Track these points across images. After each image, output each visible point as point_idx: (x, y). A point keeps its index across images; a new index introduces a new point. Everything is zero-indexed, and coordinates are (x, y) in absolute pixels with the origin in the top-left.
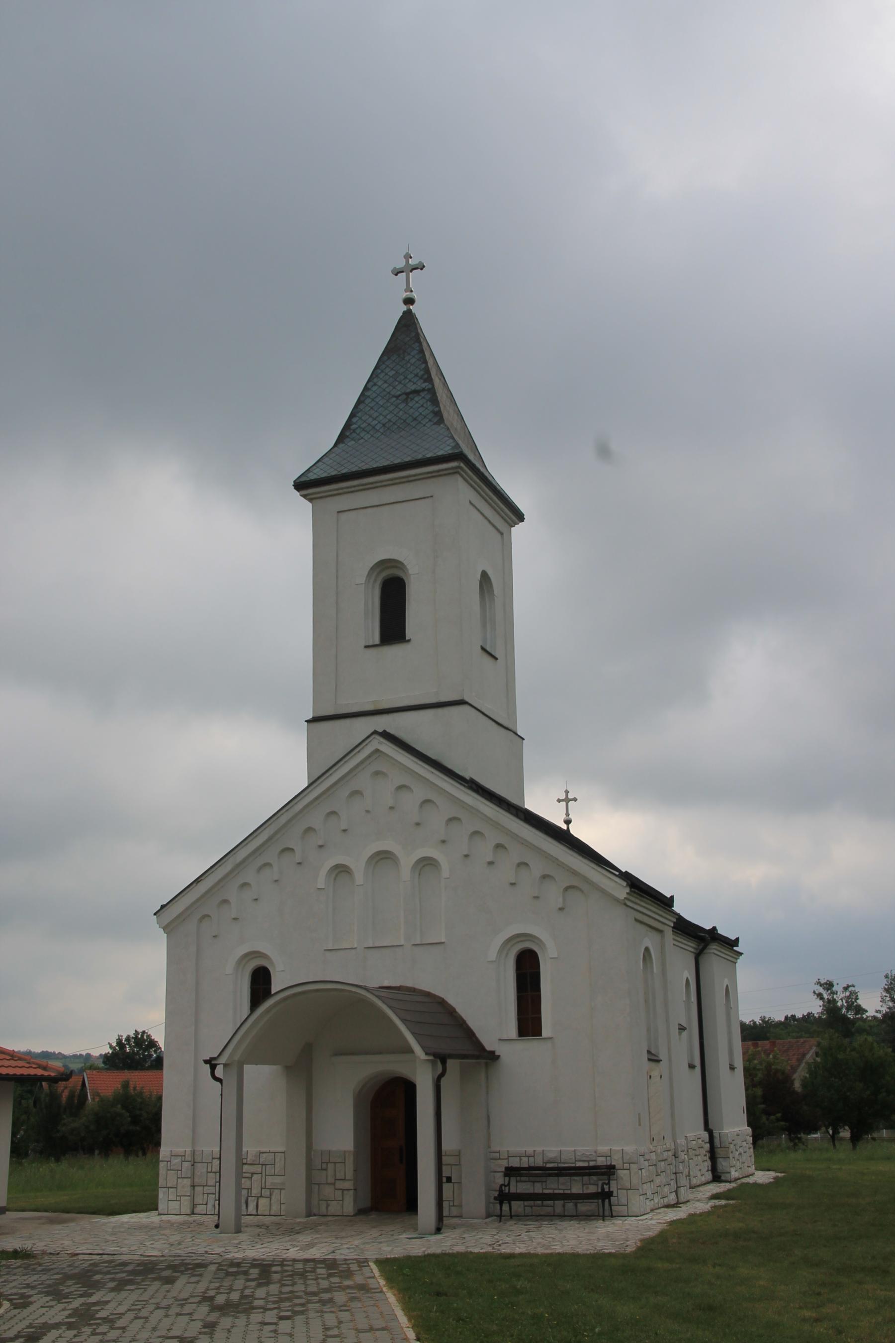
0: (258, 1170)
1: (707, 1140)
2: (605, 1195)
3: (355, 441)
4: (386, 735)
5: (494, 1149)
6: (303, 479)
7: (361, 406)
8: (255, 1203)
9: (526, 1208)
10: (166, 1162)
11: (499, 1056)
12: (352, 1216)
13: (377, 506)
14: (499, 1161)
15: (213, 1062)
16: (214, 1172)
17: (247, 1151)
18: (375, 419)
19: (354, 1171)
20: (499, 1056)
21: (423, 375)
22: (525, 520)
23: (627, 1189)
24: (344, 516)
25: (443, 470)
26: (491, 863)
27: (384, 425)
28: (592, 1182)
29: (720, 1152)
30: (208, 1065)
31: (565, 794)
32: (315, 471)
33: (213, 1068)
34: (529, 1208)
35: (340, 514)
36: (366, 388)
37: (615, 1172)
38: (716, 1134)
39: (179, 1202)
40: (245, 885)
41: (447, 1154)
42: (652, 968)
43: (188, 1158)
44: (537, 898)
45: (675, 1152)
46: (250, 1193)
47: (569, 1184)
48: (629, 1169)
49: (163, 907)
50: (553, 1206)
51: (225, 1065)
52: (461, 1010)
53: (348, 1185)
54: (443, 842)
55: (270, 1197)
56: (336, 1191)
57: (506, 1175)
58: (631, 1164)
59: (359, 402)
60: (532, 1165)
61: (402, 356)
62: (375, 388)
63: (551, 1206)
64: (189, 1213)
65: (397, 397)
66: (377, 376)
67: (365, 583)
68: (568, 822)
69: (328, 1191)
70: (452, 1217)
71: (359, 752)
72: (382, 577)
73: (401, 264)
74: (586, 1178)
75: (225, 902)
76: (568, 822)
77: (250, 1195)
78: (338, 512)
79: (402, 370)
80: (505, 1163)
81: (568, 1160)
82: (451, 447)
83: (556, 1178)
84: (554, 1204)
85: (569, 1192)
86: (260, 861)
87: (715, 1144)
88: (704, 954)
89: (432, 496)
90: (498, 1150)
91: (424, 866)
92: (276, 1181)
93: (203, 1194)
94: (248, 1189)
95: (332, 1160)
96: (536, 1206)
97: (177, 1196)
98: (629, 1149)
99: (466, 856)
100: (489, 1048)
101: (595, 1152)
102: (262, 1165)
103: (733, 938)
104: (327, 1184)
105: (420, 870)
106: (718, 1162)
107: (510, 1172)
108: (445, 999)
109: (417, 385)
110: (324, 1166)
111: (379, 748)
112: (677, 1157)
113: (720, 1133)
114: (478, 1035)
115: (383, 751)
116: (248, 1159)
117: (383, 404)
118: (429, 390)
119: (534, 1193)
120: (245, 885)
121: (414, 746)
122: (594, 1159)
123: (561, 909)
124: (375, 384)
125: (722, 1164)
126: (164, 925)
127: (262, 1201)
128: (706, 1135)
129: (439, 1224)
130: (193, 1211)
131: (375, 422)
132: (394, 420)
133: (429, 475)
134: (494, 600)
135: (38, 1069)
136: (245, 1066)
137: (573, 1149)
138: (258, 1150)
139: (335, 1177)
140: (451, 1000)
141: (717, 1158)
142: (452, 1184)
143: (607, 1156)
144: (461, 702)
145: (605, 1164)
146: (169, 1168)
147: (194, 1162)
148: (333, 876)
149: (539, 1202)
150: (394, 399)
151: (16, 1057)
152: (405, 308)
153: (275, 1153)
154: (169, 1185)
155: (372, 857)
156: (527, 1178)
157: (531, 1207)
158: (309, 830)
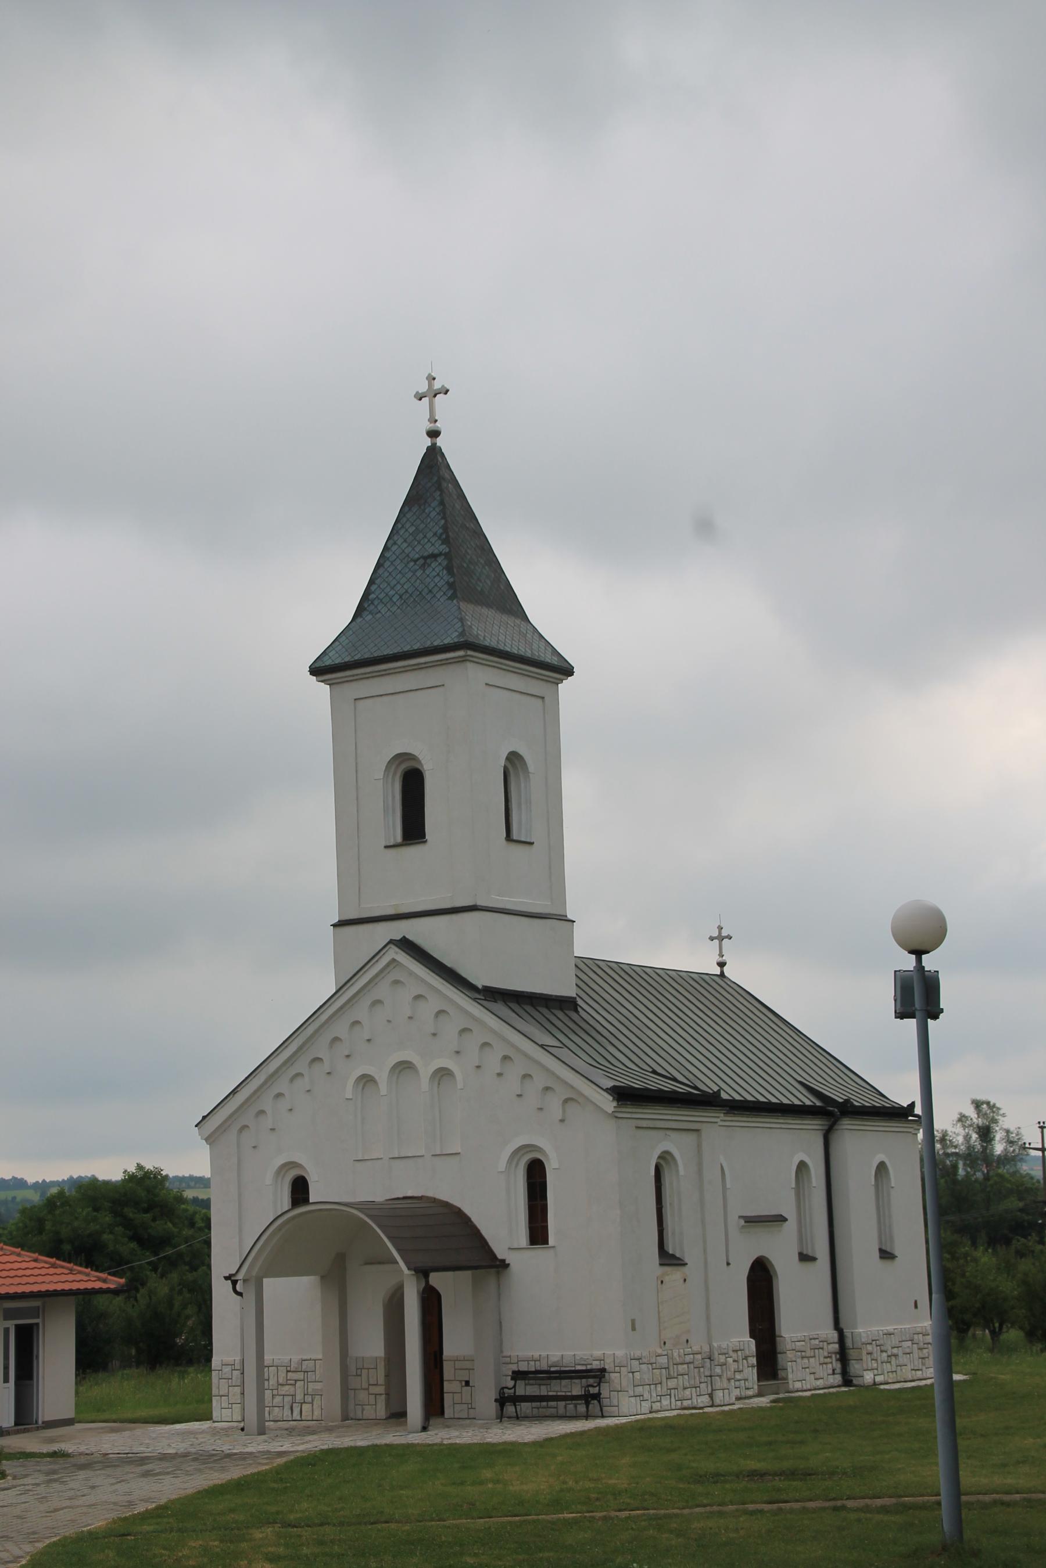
1: (836, 1339)
2: (590, 1397)
3: (372, 614)
4: (407, 945)
5: (505, 1354)
7: (381, 571)
8: (299, 1408)
9: (534, 1409)
10: (218, 1372)
11: (509, 1265)
12: (385, 1419)
13: (392, 694)
14: (510, 1365)
15: (233, 1278)
17: (291, 1359)
18: (392, 588)
19: (386, 1376)
20: (509, 1265)
21: (441, 534)
22: (574, 674)
23: (618, 1391)
24: (361, 703)
26: (500, 1075)
27: (401, 597)
29: (852, 1354)
30: (230, 1281)
31: (717, 930)
32: (331, 654)
33: (235, 1283)
34: (536, 1409)
35: (357, 701)
36: (386, 548)
38: (847, 1332)
39: (231, 1410)
40: (279, 1095)
42: (677, 1171)
43: (237, 1367)
44: (541, 1109)
45: (711, 1355)
47: (570, 1386)
48: (620, 1372)
49: (204, 1118)
51: (245, 1281)
52: (476, 1220)
53: (381, 1390)
54: (458, 1052)
55: (312, 1403)
56: (370, 1396)
57: (512, 1379)
58: (622, 1368)
60: (539, 1369)
61: (422, 507)
64: (240, 1420)
65: (415, 561)
66: (397, 532)
67: (383, 779)
68: (721, 965)
69: (362, 1396)
71: (377, 961)
72: (403, 768)
73: (423, 388)
75: (262, 1112)
76: (721, 965)
78: (355, 699)
79: (422, 526)
80: (515, 1368)
81: (568, 1365)
82: (457, 634)
85: (569, 1394)
86: (292, 1072)
87: (847, 1345)
88: (837, 1130)
90: (509, 1354)
92: (316, 1388)
94: (292, 1395)
95: (365, 1366)
96: (542, 1408)
98: (620, 1353)
99: (478, 1067)
100: (500, 1256)
101: (592, 1356)
102: (304, 1372)
103: (905, 1104)
105: (440, 1080)
106: (851, 1365)
107: (517, 1375)
108: (462, 1209)
109: (435, 546)
111: (395, 958)
112: (713, 1360)
113: (852, 1332)
114: (490, 1244)
116: (292, 1367)
117: (402, 570)
118: (446, 555)
120: (279, 1095)
121: (431, 953)
122: (590, 1363)
124: (395, 543)
125: (855, 1367)
126: (205, 1137)
127: (305, 1407)
128: (834, 1335)
129: (425, 1423)
131: (392, 593)
133: (439, 663)
134: (529, 776)
135: (98, 1282)
136: (264, 1279)
138: (301, 1357)
139: (369, 1382)
140: (467, 1210)
141: (849, 1360)
146: (220, 1377)
148: (361, 1085)
150: (412, 564)
151: (74, 1271)
152: (428, 442)
153: (315, 1360)
154: (221, 1393)
157: (538, 1408)
158: (336, 1039)
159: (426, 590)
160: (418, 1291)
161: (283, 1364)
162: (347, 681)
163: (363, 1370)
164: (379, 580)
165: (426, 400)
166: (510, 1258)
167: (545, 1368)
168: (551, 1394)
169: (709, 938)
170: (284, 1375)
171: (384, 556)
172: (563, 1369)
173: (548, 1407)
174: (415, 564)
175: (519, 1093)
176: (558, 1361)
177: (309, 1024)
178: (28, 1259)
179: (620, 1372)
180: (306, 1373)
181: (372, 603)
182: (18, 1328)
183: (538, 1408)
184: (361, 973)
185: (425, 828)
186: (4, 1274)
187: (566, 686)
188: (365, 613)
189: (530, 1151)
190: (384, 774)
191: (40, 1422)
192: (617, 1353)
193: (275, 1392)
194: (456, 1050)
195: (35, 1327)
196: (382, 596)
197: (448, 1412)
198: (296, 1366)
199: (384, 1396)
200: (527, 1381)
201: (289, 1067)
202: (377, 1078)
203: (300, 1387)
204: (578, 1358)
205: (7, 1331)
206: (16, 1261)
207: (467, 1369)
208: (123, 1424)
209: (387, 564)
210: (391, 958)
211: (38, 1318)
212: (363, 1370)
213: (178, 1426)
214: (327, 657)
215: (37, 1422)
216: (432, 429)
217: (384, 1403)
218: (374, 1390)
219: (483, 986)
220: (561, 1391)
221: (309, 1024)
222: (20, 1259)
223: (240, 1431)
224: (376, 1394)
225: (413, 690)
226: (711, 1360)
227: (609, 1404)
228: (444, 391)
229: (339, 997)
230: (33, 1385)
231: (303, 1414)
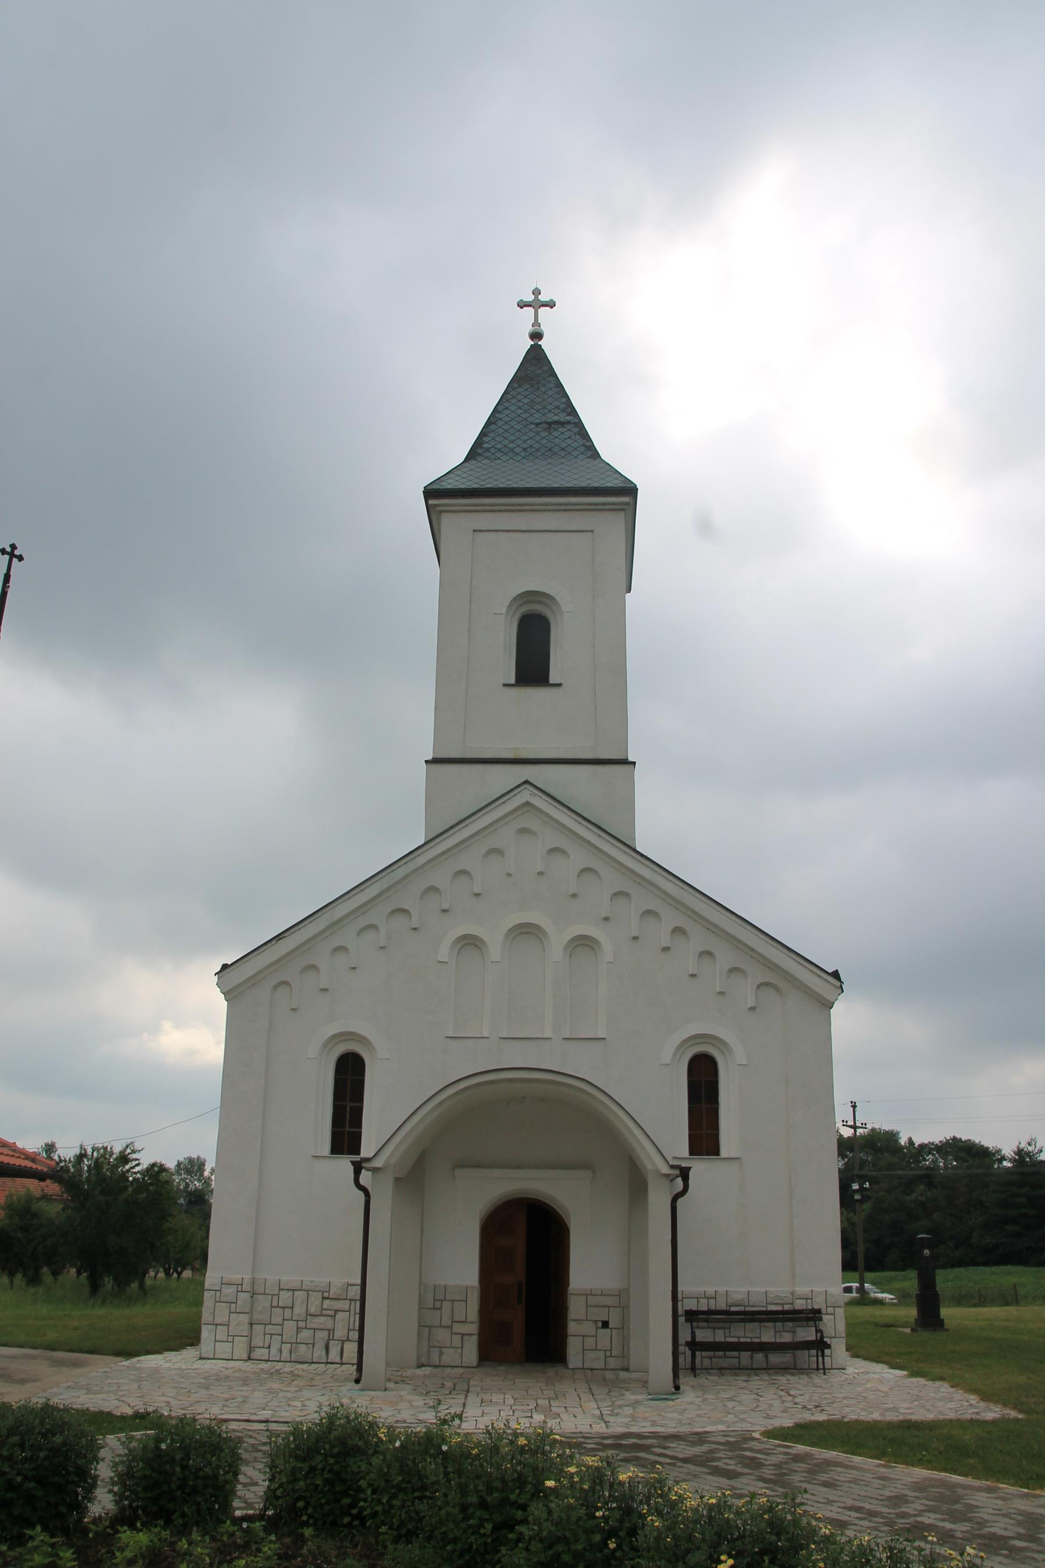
0: (345, 1306)
3: (489, 459)
6: (436, 487)
8: (339, 1348)
9: (704, 1359)
16: (280, 1307)
18: (512, 442)
25: (609, 504)
26: (666, 949)
28: (787, 1329)
34: (708, 1360)
35: (476, 533)
37: (822, 1317)
40: (341, 949)
41: (604, 1293)
46: (331, 1335)
47: (758, 1331)
50: (739, 1358)
54: (606, 919)
58: (836, 1309)
59: (489, 423)
62: (507, 412)
63: (736, 1358)
65: (537, 425)
70: (607, 1369)
74: (779, 1324)
77: (331, 1338)
78: (474, 531)
83: (743, 1324)
84: (739, 1354)
85: (758, 1340)
86: (363, 922)
89: (592, 531)
91: (576, 946)
93: (265, 1334)
94: (329, 1330)
97: (228, 1336)
99: (635, 938)
102: (351, 1300)
104: (441, 1326)
110: (438, 1304)
115: (536, 805)
116: (331, 1293)
119: (714, 1342)
120: (341, 949)
123: (752, 1009)
124: (507, 408)
127: (347, 1345)
130: (249, 1357)
132: (537, 446)
137: (764, 1290)
138: (347, 1281)
142: (609, 1330)
143: (807, 1299)
145: (805, 1308)
147: (254, 1294)
149: (721, 1353)
150: (534, 426)
154: (218, 1320)
155: (510, 931)
156: (707, 1324)
161: (318, 1289)
162: (466, 511)
163: (445, 1303)
167: (724, 1307)
170: (318, 1302)
171: (494, 416)
172: (748, 1309)
177: (399, 867)
179: (834, 1314)
183: (711, 1358)
184: (481, 814)
189: (698, 1043)
193: (302, 1324)
197: (574, 1357)
198: (339, 1291)
201: (359, 916)
207: (605, 1306)
212: (445, 1303)
218: (458, 1328)
220: (745, 1337)
221: (399, 867)
223: (353, 1383)
225: (551, 531)
229: (447, 838)
231: (344, 1355)
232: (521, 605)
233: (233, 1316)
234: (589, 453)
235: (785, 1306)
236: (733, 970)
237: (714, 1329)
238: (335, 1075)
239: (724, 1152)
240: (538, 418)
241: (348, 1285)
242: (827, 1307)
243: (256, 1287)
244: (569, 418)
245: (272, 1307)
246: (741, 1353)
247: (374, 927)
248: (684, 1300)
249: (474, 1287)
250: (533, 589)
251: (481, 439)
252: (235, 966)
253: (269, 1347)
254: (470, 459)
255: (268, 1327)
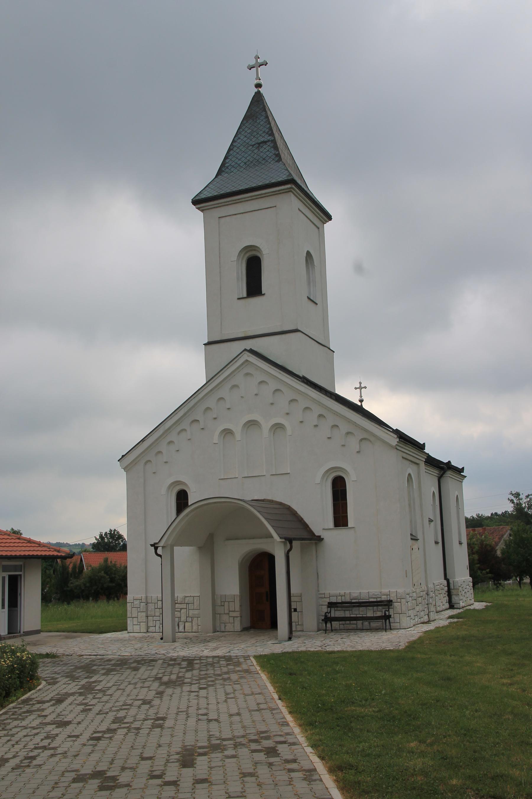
1: (446, 585)
6: (197, 198)
7: (231, 152)
14: (324, 599)
18: (239, 160)
20: (323, 539)
21: (268, 132)
24: (222, 220)
26: (316, 426)
27: (245, 163)
28: (379, 610)
29: (453, 592)
30: (153, 547)
33: (156, 549)
35: (220, 219)
38: (451, 581)
39: (139, 626)
40: (171, 442)
47: (366, 611)
49: (123, 456)
51: (163, 547)
53: (237, 614)
54: (288, 414)
57: (328, 607)
59: (230, 150)
60: (344, 601)
61: (255, 120)
65: (253, 146)
66: (240, 133)
69: (225, 618)
71: (236, 362)
73: (253, 62)
74: (375, 608)
75: (160, 452)
76: (361, 401)
78: (219, 218)
79: (255, 129)
81: (364, 598)
85: (366, 616)
86: (179, 428)
87: (451, 587)
92: (195, 613)
93: (153, 621)
98: (400, 591)
99: (301, 422)
102: (187, 604)
104: (225, 614)
107: (331, 605)
110: (223, 604)
120: (171, 442)
123: (358, 452)
124: (239, 138)
125: (455, 599)
127: (187, 624)
128: (445, 582)
131: (240, 162)
135: (55, 552)
140: (294, 507)
143: (387, 595)
144: (297, 331)
146: (133, 607)
147: (147, 603)
149: (348, 622)
150: (251, 147)
152: (256, 90)
156: (341, 608)
157: (344, 625)
158: (208, 409)
159: (261, 159)
160: (285, 552)
162: (214, 208)
163: (225, 603)
164: (230, 157)
165: (254, 70)
166: (323, 534)
167: (349, 600)
168: (352, 616)
169: (355, 388)
171: (233, 144)
173: (350, 624)
174: (253, 147)
175: (329, 436)
176: (357, 596)
178: (15, 538)
179: (401, 602)
180: (188, 605)
181: (227, 168)
182: (10, 577)
183: (344, 625)
185: (261, 289)
186: (3, 545)
187: (328, 226)
188: (223, 174)
189: (335, 471)
190: (237, 258)
191: (22, 632)
192: (399, 591)
194: (287, 412)
195: (19, 577)
196: (233, 164)
198: (181, 600)
199: (239, 618)
200: (336, 609)
202: (234, 430)
203: (184, 613)
204: (371, 594)
205: (4, 578)
206: (8, 539)
208: (68, 633)
209: (235, 149)
210: (245, 359)
211: (21, 571)
212: (225, 603)
213: (109, 635)
214: (202, 195)
215: (20, 632)
216: (258, 83)
217: (239, 623)
218: (232, 614)
219: (303, 376)
220: (359, 614)
222: (10, 538)
224: (234, 617)
226: (428, 595)
227: (393, 622)
228: (266, 64)
230: (17, 611)
232: (245, 253)
233: (139, 613)
234: (277, 159)
235: (378, 599)
236: (348, 433)
237: (345, 610)
238: (177, 501)
239: (350, 525)
240: (254, 141)
241: (185, 597)
242: (397, 599)
243: (148, 600)
244: (269, 138)
245: (155, 608)
246: (358, 621)
247: (184, 430)
248: (330, 597)
249: (237, 595)
250: (249, 245)
251: (225, 161)
252: (126, 456)
253: (155, 626)
254: (218, 176)
255: (154, 617)
